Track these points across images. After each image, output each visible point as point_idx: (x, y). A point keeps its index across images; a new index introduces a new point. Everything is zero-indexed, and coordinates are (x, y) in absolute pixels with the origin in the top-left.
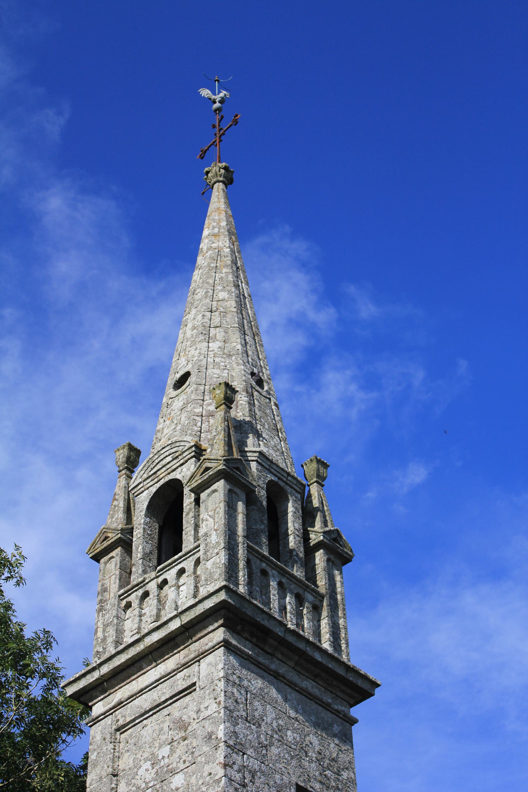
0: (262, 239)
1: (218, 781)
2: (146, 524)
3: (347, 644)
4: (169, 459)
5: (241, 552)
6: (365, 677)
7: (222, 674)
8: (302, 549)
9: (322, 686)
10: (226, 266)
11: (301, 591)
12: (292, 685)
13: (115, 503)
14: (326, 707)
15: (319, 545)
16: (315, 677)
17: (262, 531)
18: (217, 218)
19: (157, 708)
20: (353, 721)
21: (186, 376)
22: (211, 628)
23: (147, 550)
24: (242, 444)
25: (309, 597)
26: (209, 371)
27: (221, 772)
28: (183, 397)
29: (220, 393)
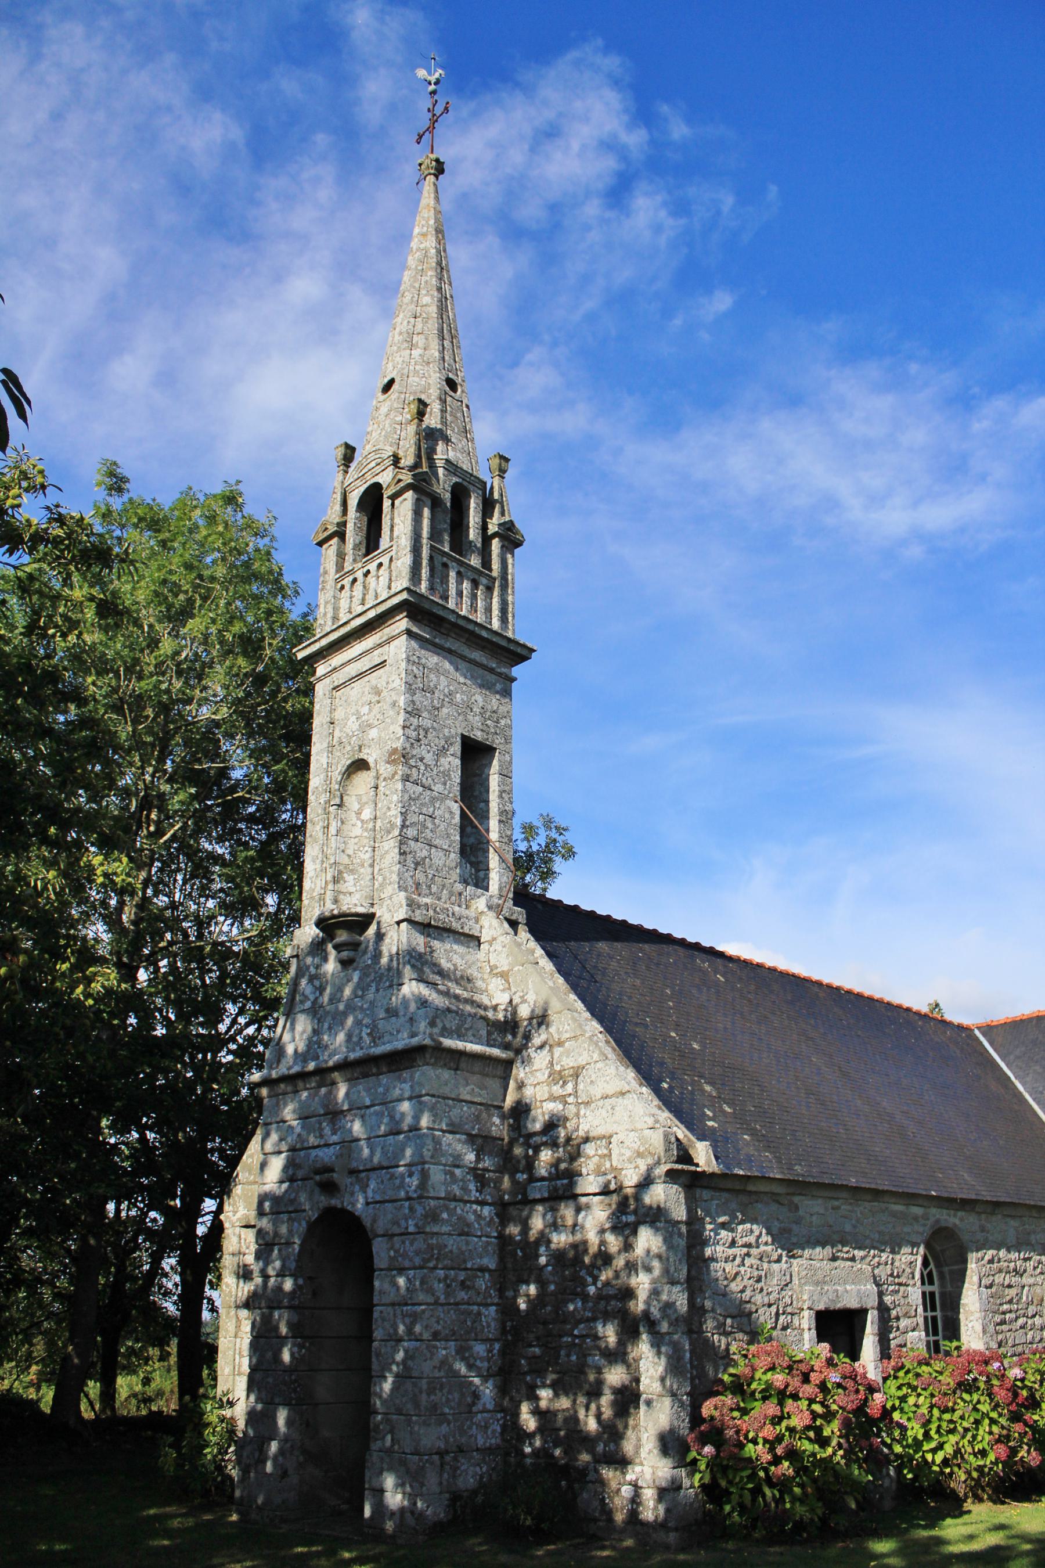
0: (573, 55)
1: (399, 739)
2: (356, 518)
3: (513, 616)
4: (373, 464)
5: (424, 552)
6: (524, 646)
7: (404, 656)
8: (480, 540)
10: (431, 268)
11: (476, 577)
12: (463, 658)
13: (335, 496)
14: (491, 671)
15: (495, 535)
16: (483, 648)
17: (445, 530)
18: (426, 215)
19: (360, 675)
20: (513, 680)
21: (392, 382)
22: (398, 618)
23: (357, 542)
24: (431, 451)
25: (484, 581)
26: (410, 379)
27: (401, 732)
28: (388, 403)
29: (414, 407)
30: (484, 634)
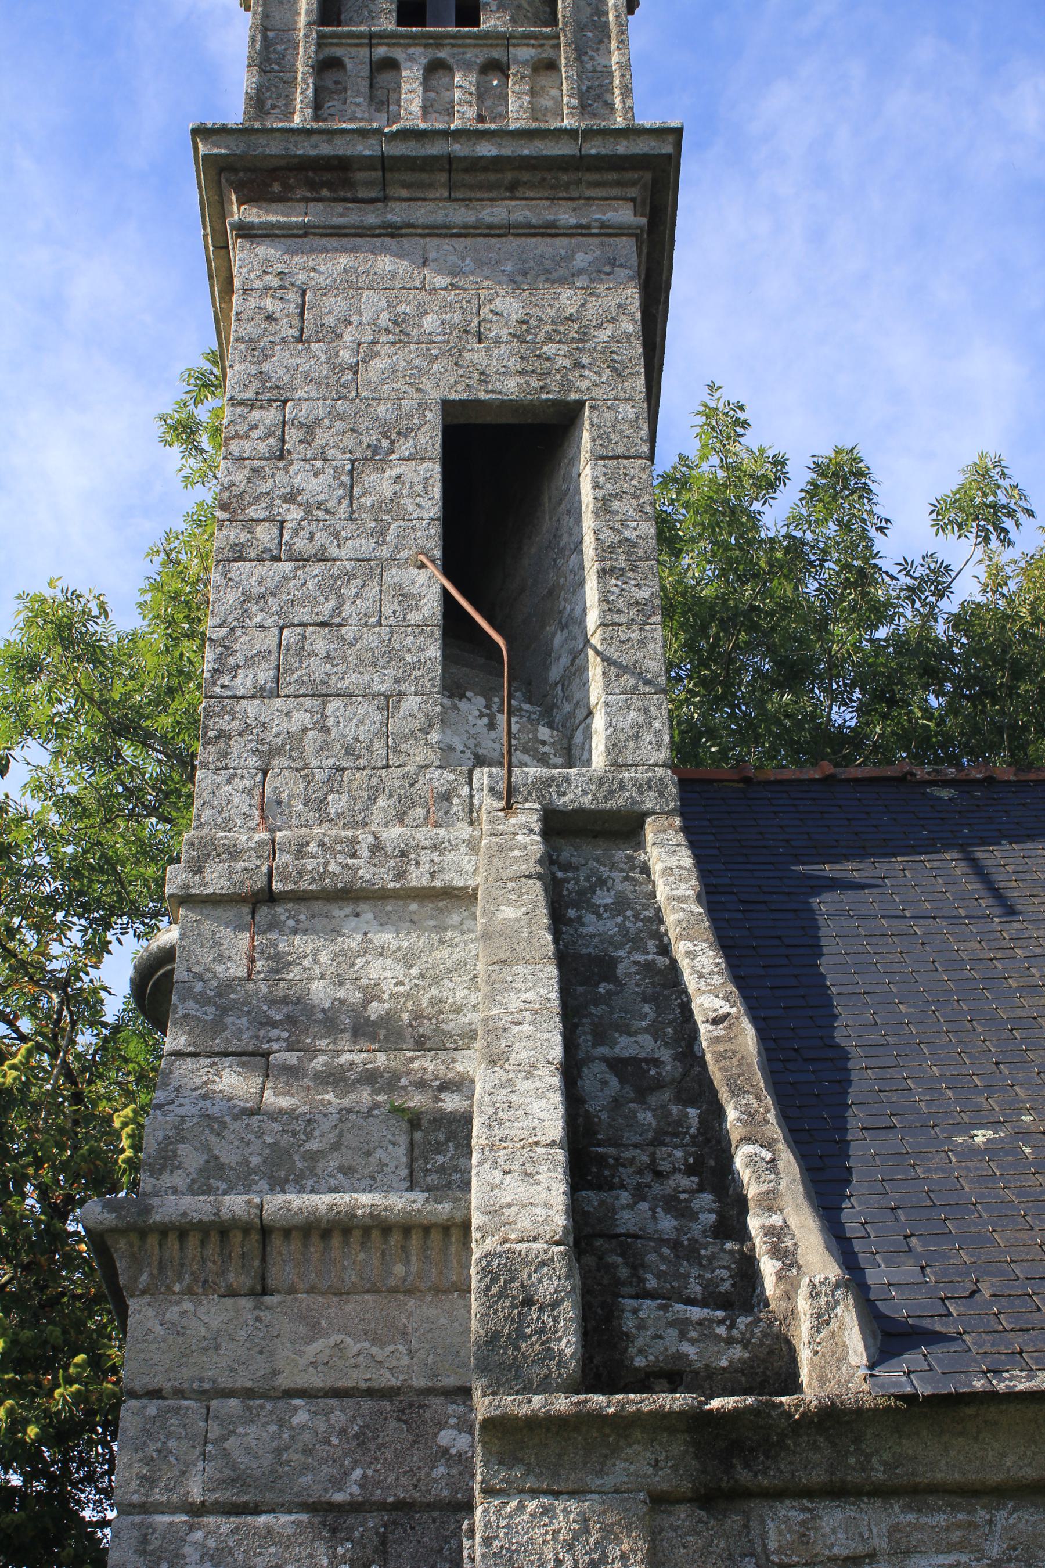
9: (540, 199)
14: (549, 230)
16: (512, 189)
30: (486, 149)
